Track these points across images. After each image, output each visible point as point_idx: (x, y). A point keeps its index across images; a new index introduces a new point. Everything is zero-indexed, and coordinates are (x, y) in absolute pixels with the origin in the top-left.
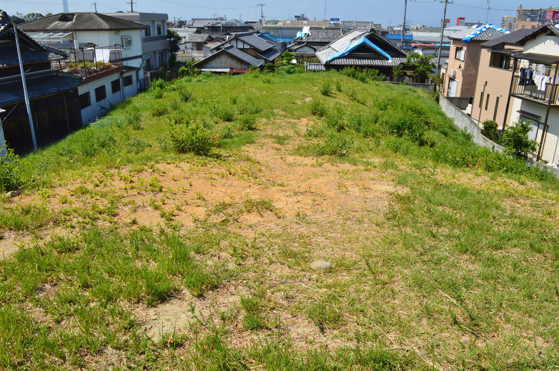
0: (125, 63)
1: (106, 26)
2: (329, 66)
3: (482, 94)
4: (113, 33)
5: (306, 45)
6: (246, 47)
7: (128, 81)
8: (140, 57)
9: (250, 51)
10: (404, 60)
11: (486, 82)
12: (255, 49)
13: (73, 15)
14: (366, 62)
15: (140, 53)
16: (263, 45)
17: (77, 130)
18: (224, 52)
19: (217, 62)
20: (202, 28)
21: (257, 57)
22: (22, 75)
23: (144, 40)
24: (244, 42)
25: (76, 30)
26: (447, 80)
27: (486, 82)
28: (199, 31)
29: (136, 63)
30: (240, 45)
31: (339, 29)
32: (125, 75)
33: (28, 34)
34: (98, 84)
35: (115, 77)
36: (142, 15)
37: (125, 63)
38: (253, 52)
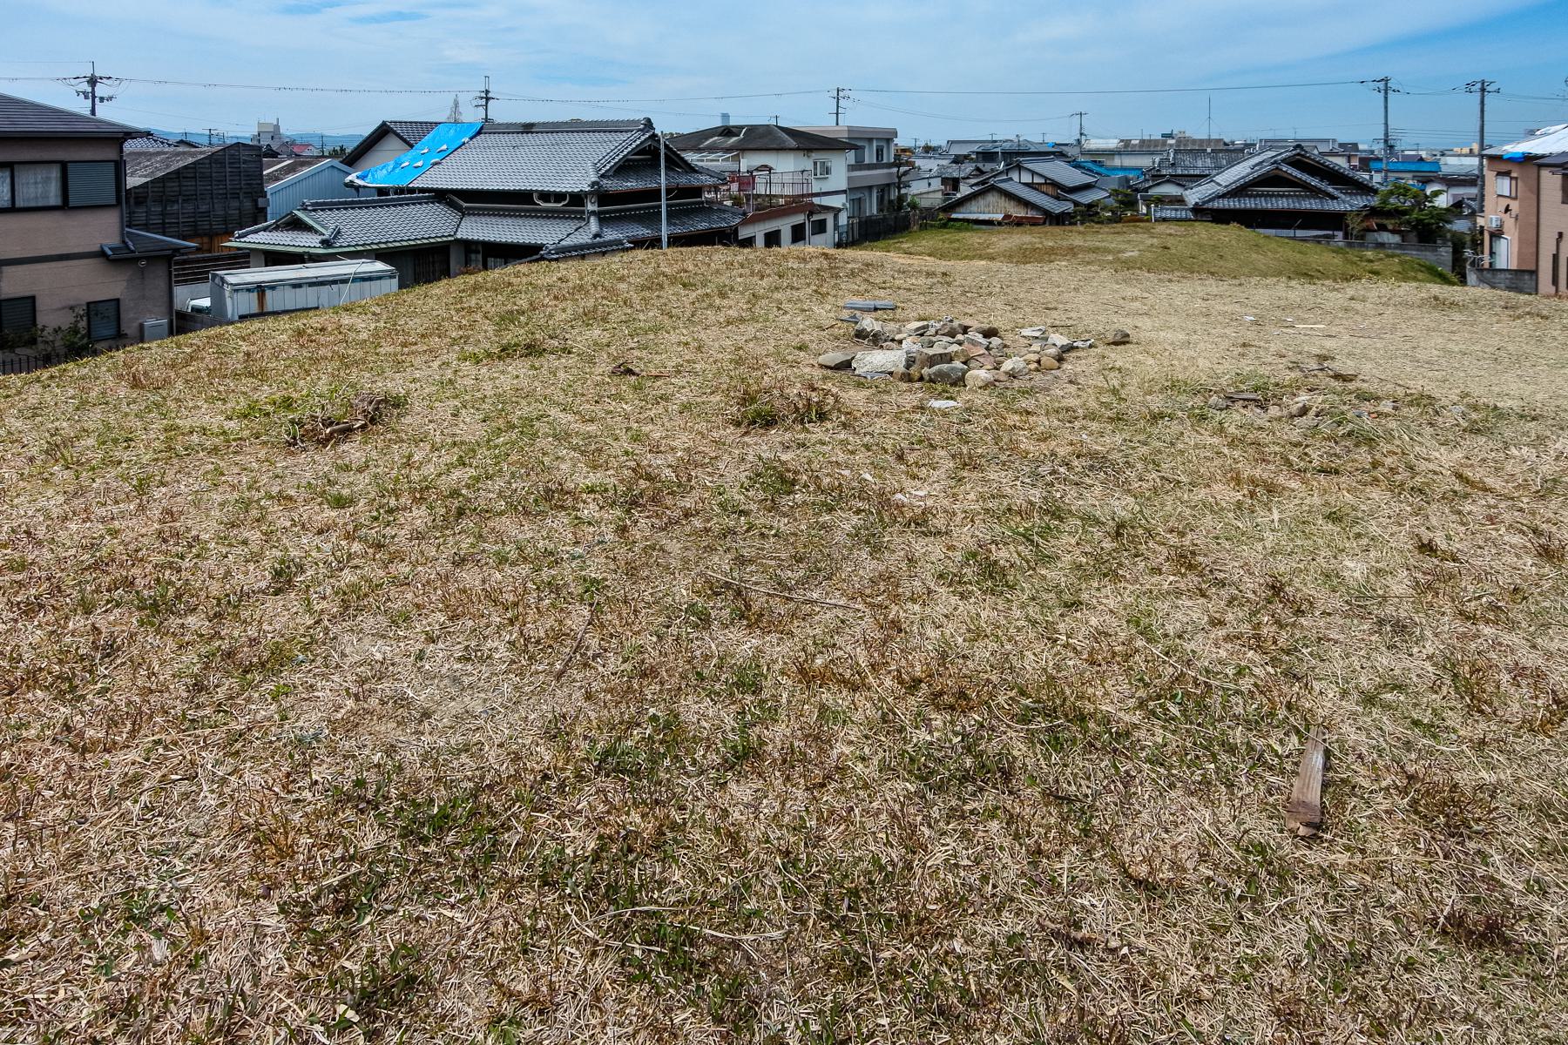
0: (816, 200)
1: (792, 143)
2: (1202, 213)
3: (1556, 258)
4: (801, 154)
5: (1168, 181)
6: (1037, 180)
7: (820, 227)
8: (844, 192)
9: (1044, 188)
10: (1375, 201)
11: (1561, 235)
12: (1055, 185)
13: (742, 127)
14: (1283, 204)
15: (844, 187)
16: (1072, 177)
17: (707, 244)
18: (993, 188)
19: (981, 202)
20: (966, 157)
21: (1057, 198)
22: (664, 202)
23: (851, 168)
24: (1033, 173)
25: (744, 150)
26: (1487, 237)
27: (1561, 235)
28: (958, 160)
29: (837, 201)
30: (1026, 178)
31: (1231, 152)
32: (815, 218)
33: (684, 155)
34: (770, 226)
35: (799, 219)
36: (850, 130)
37: (816, 200)
38: (1050, 190)
